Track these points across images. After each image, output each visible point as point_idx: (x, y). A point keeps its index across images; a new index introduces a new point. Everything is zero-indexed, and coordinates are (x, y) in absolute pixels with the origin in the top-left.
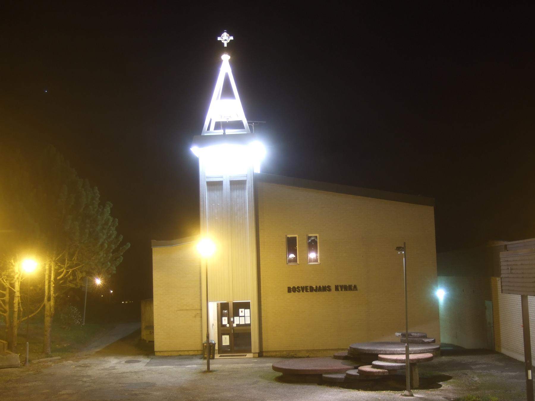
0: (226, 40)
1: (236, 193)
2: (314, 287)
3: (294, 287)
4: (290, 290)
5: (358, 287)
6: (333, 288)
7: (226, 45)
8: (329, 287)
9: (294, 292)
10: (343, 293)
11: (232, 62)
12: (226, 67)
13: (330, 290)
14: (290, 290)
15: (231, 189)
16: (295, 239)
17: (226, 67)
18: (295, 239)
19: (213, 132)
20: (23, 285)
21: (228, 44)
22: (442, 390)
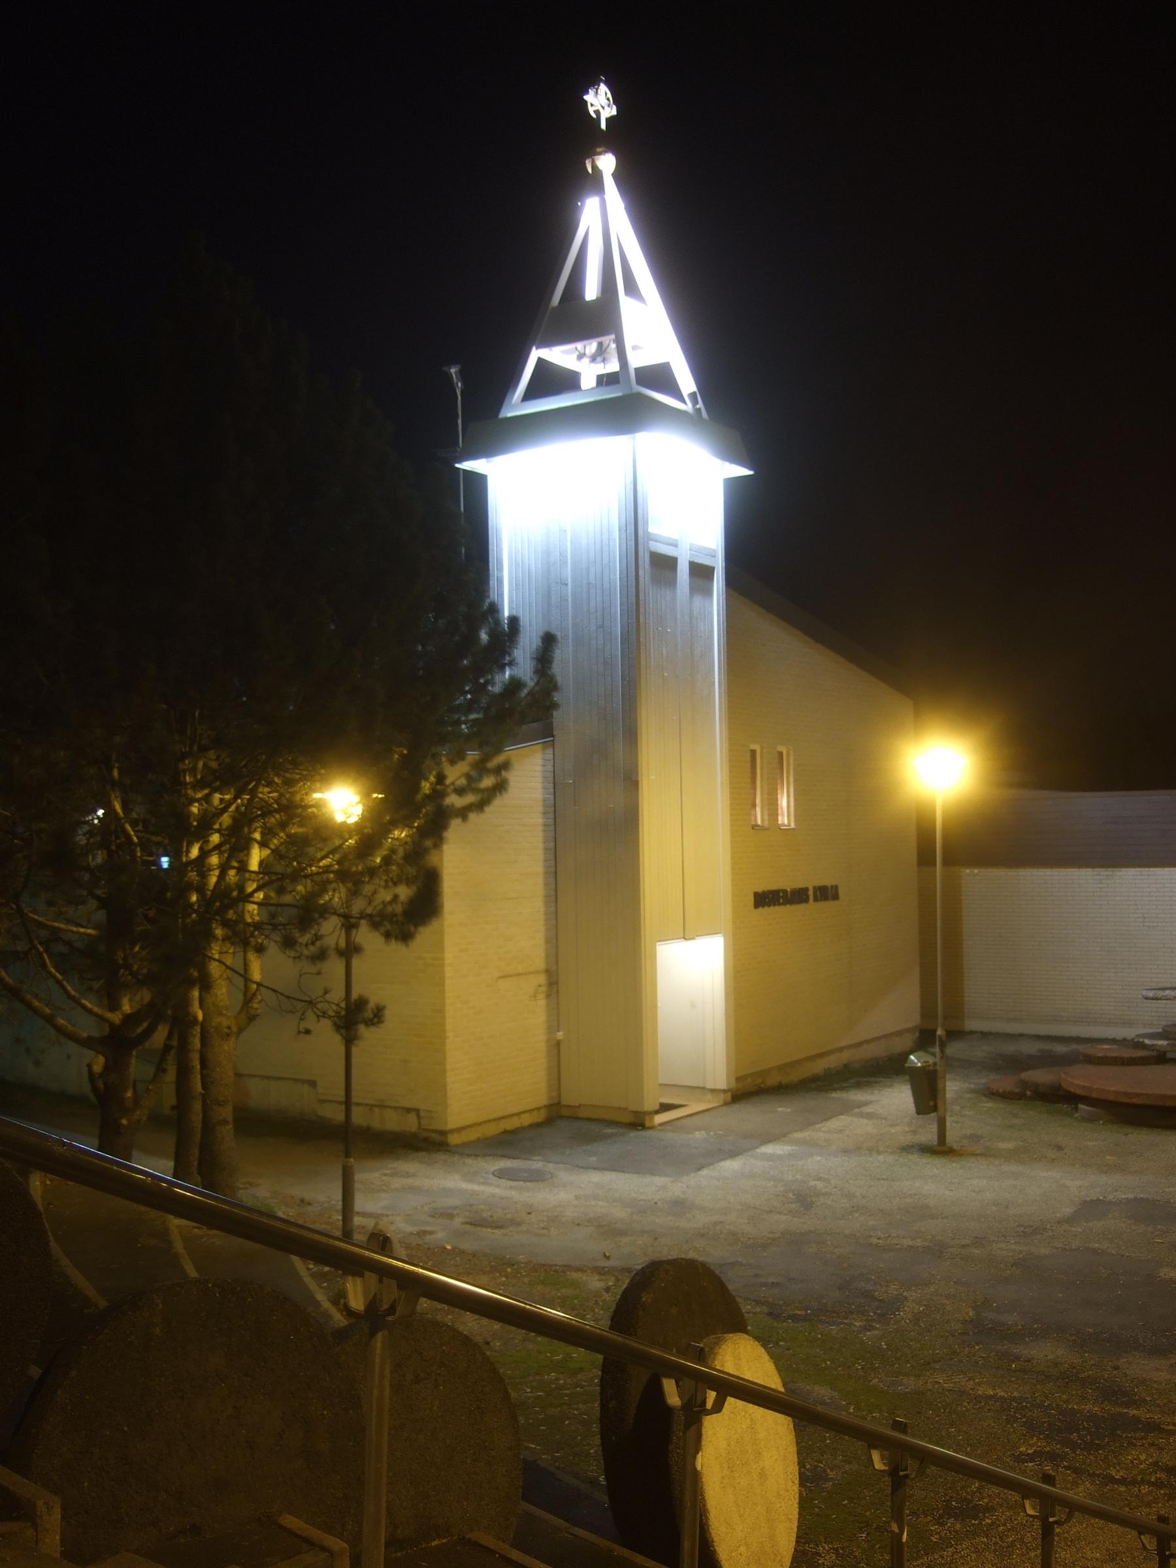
1: (698, 601)
7: (603, 126)
13: (806, 900)
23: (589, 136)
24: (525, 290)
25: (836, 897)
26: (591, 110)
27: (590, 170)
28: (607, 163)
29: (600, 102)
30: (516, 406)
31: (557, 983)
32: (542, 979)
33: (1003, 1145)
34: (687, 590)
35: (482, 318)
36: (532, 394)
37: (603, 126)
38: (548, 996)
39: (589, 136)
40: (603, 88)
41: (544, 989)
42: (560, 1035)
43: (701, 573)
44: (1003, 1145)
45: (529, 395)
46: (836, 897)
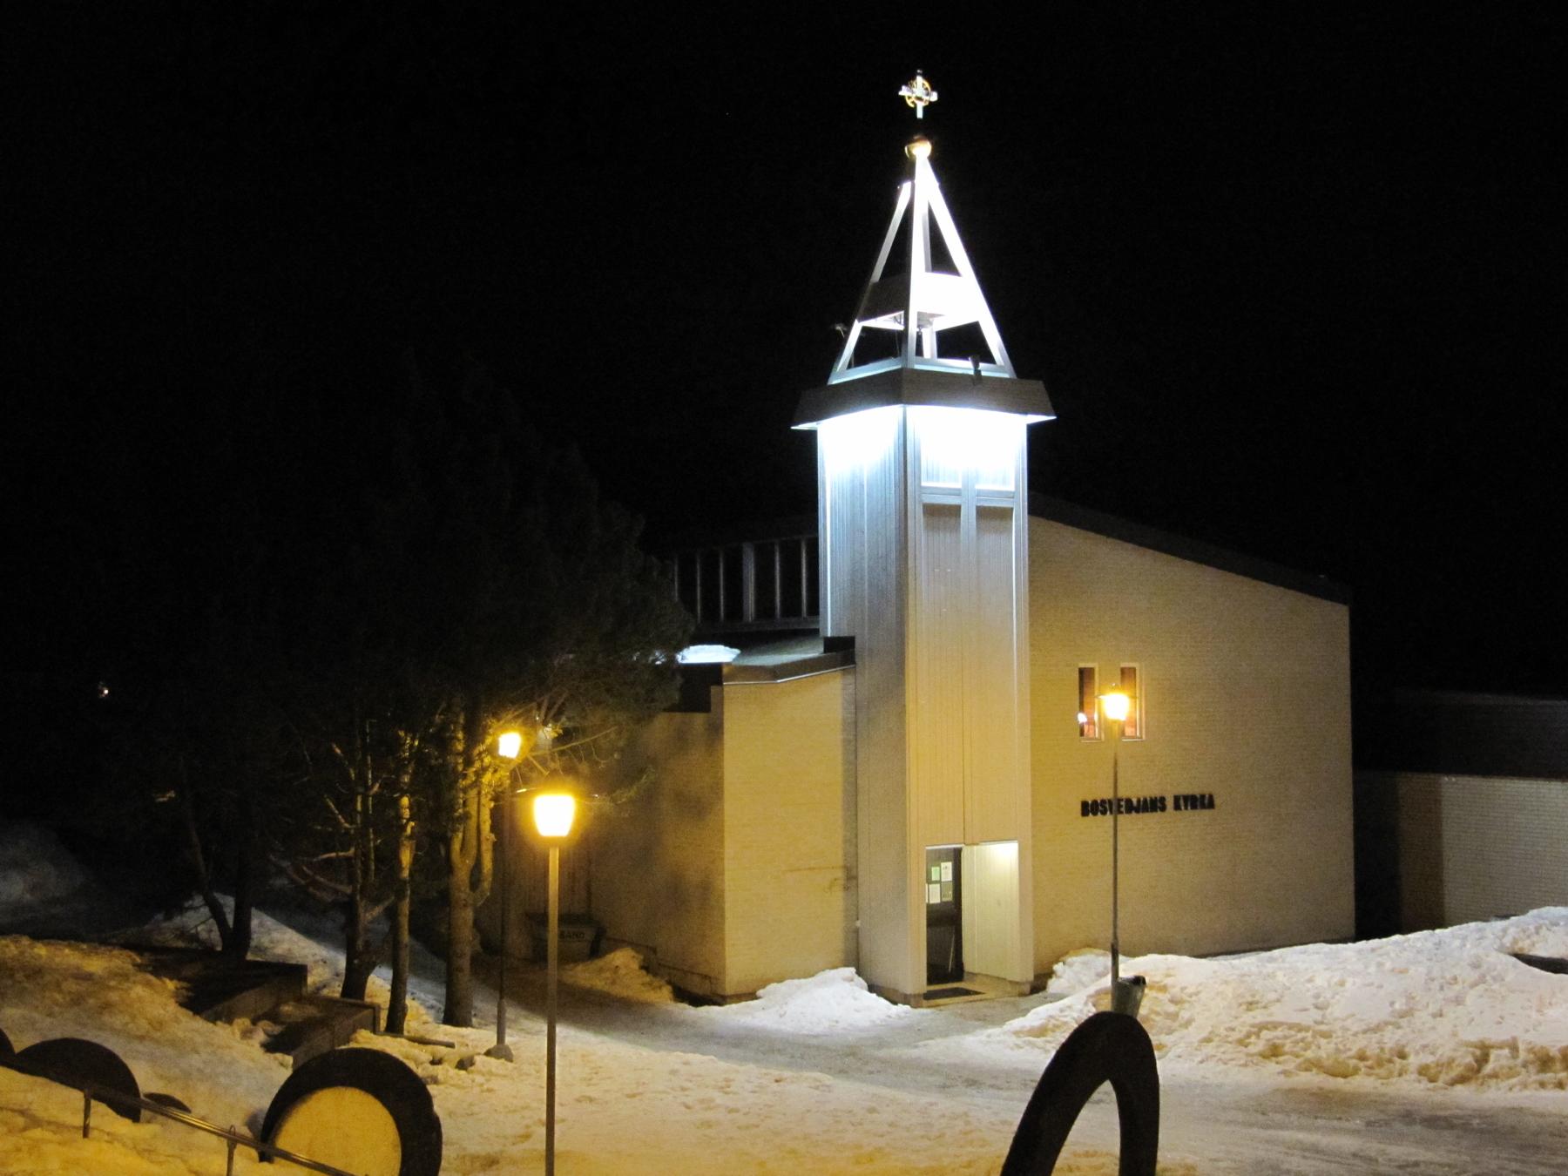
0: (920, 99)
1: (990, 540)
2: (1135, 801)
3: (1095, 802)
4: (1089, 808)
5: (1217, 801)
6: (1170, 803)
7: (920, 114)
8: (1163, 799)
9: (1095, 814)
10: (1188, 814)
11: (937, 161)
12: (923, 194)
13: (1163, 809)
14: (1089, 808)
15: (978, 528)
16: (1091, 671)
17: (923, 194)
18: (1091, 671)
19: (931, 360)
20: (812, 435)
21: (925, 109)
22: (1495, 1076)
23: (905, 124)
24: (852, 264)
25: (1211, 805)
26: (909, 102)
27: (359, 808)
28: (921, 151)
29: (918, 94)
30: (843, 373)
31: (856, 878)
32: (840, 874)
33: (443, 852)
34: (973, 532)
35: (804, 308)
36: (860, 358)
37: (920, 114)
38: (846, 888)
39: (905, 124)
40: (920, 80)
41: (841, 882)
42: (858, 923)
43: (992, 516)
44: (443, 852)
45: (860, 358)
46: (1211, 805)
